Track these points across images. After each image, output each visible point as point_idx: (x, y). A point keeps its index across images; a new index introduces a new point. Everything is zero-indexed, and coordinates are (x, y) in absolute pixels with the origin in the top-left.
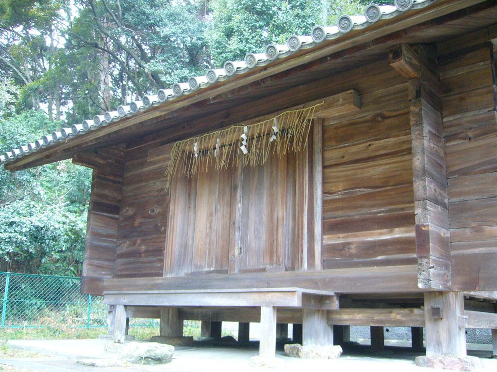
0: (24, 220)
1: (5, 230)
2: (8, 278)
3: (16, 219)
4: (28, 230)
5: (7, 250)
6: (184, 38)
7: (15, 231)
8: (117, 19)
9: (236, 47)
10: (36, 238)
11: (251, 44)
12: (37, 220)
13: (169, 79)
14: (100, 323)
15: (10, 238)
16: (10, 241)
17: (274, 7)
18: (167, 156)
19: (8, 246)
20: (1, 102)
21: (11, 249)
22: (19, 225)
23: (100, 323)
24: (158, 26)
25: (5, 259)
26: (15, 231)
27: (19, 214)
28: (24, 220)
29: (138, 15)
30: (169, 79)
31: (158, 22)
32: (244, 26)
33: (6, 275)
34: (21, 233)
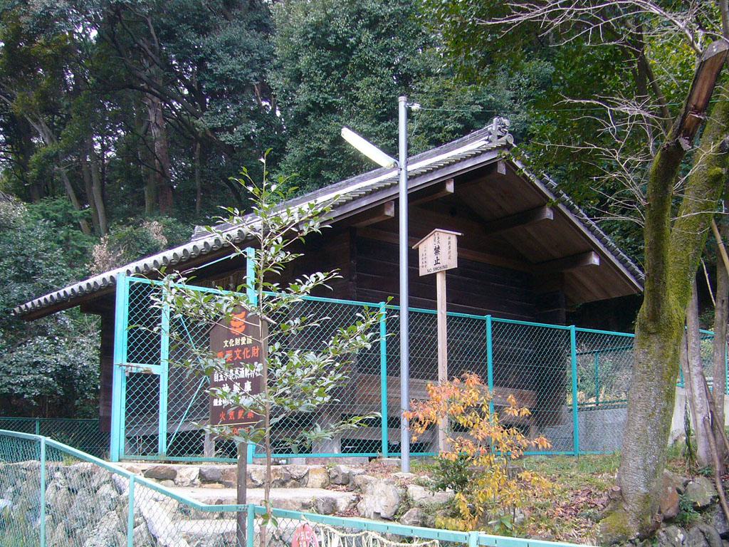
0: (48, 358)
1: (29, 372)
2: (37, 424)
3: (40, 359)
4: (54, 370)
5: (33, 394)
6: (246, 75)
7: (40, 373)
8: (154, 53)
9: (306, 99)
10: (64, 378)
11: (326, 93)
12: (65, 356)
13: (230, 138)
14: (424, 518)
15: (35, 379)
16: (36, 384)
17: (351, 37)
18: (538, 7)
19: (33, 389)
20: (58, 2)
21: (36, 392)
22: (44, 365)
23: (424, 518)
24: (210, 61)
25: (32, 403)
26: (40, 373)
27: (43, 352)
28: (48, 358)
29: (181, 48)
30: (230, 138)
31: (210, 55)
32: (316, 69)
33: (35, 421)
34: (46, 374)
